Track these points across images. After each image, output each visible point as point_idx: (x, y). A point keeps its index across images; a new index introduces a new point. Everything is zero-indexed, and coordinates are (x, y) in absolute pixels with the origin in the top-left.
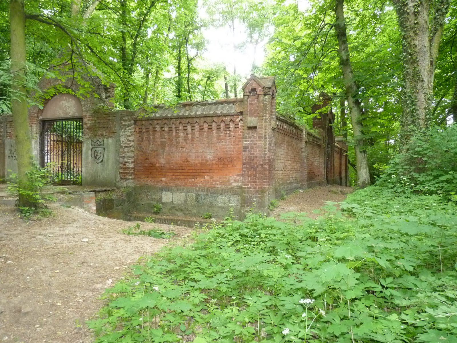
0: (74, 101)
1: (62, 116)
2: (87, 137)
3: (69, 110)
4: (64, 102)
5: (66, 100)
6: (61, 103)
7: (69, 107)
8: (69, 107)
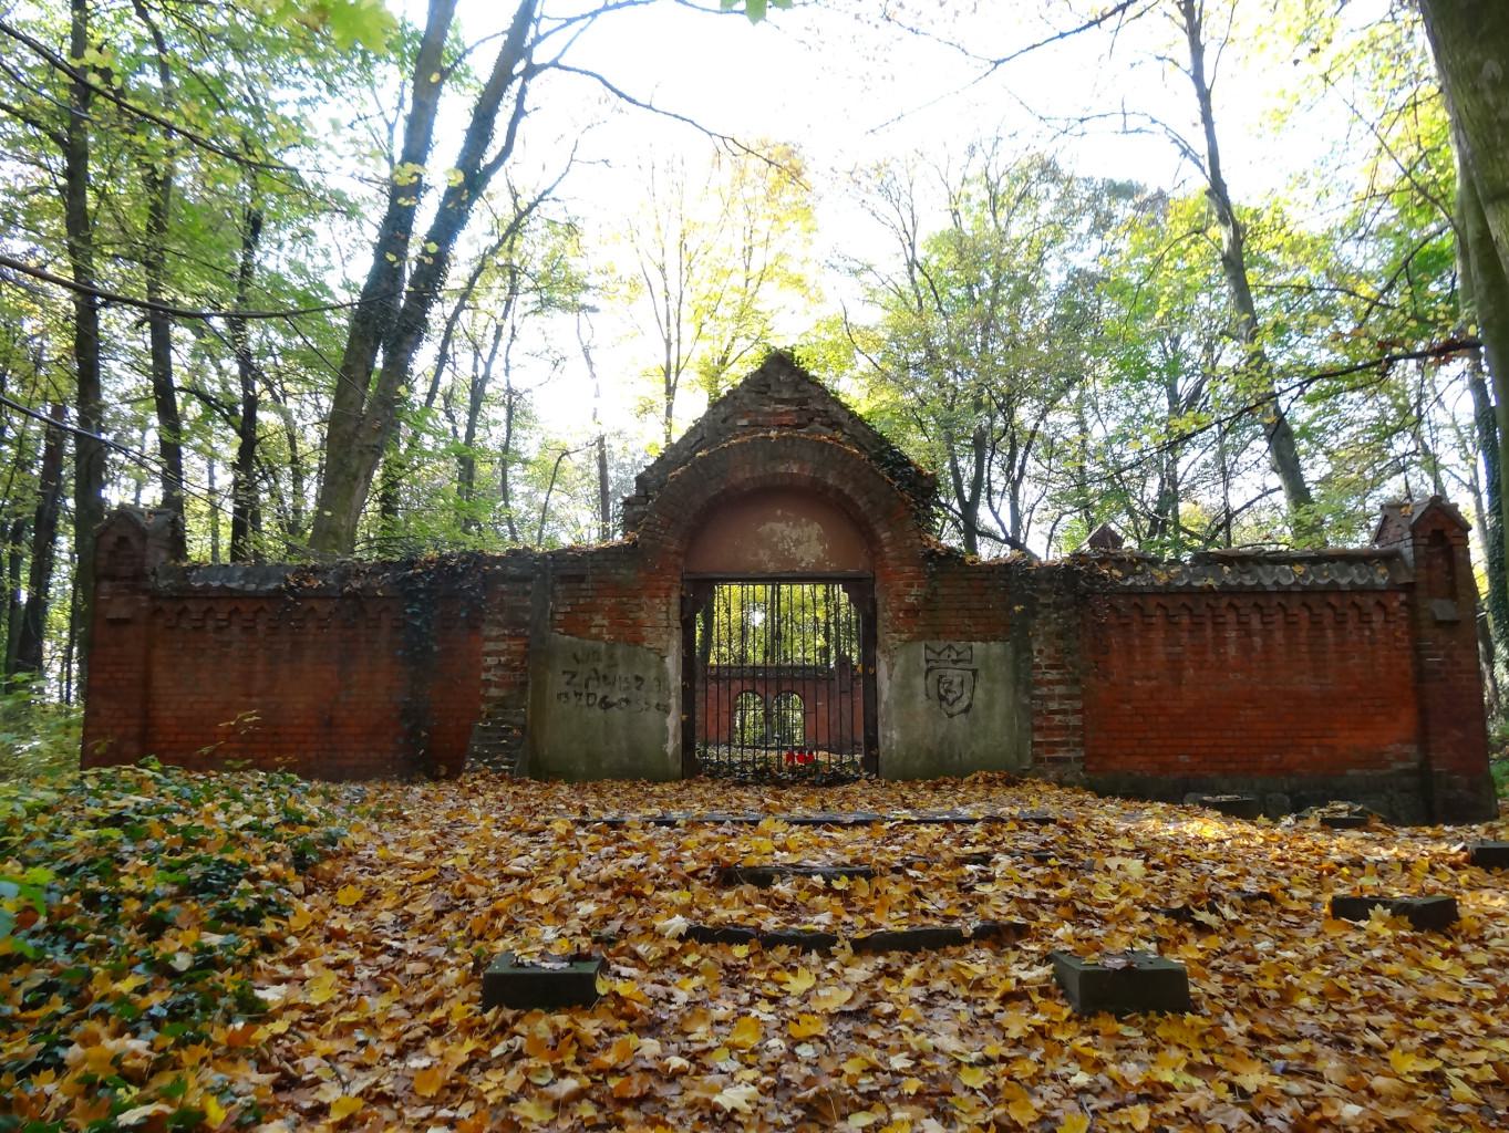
0: (817, 526)
1: (771, 567)
2: (904, 637)
3: (798, 552)
4: (779, 527)
5: (779, 520)
6: (765, 528)
7: (798, 542)
8: (798, 542)
